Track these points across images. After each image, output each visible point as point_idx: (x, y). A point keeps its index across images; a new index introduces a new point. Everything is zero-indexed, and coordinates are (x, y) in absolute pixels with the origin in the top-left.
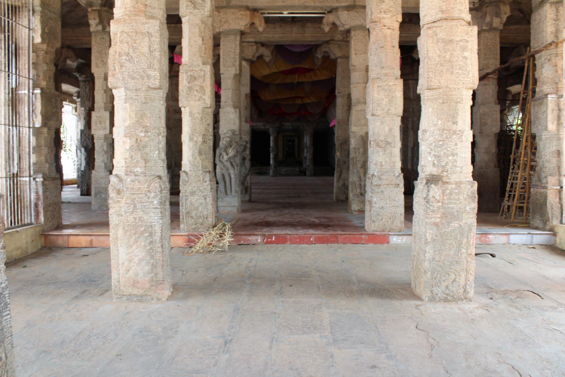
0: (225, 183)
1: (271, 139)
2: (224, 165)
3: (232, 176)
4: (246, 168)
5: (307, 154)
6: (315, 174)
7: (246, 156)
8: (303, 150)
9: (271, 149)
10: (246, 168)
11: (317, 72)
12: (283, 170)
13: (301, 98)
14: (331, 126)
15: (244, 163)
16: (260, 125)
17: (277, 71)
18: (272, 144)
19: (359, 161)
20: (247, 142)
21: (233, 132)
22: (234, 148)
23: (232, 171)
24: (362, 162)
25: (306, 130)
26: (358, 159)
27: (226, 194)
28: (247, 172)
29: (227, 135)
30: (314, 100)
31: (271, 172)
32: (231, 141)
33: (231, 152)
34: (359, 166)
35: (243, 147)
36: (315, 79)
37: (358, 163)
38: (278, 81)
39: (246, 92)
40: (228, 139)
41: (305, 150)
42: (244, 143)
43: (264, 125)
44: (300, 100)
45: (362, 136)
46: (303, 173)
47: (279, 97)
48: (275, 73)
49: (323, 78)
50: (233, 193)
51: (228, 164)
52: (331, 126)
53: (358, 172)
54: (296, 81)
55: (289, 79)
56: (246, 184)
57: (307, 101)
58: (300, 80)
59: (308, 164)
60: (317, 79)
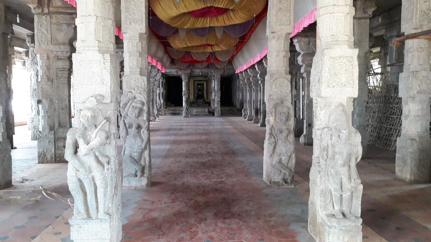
0: (85, 194)
1: (184, 84)
2: (82, 163)
3: (98, 183)
4: (143, 140)
5: (215, 97)
6: (223, 114)
7: (142, 124)
8: (212, 93)
9: (183, 93)
10: (143, 140)
11: (231, 14)
12: (194, 111)
13: (211, 46)
14: (236, 72)
15: (139, 132)
16: (173, 71)
17: (186, 11)
18: (184, 89)
19: (341, 153)
20: (143, 104)
21: (100, 99)
22: (101, 130)
23: (97, 173)
24: (345, 155)
25: (214, 76)
26: (336, 150)
27: (89, 217)
28: (143, 146)
29: (89, 105)
30: (224, 48)
31: (184, 115)
32: (94, 117)
33: (96, 138)
34: (340, 162)
35: (137, 111)
36: (228, 23)
37: (337, 156)
38: (188, 26)
39: (140, 31)
40: (89, 114)
41: (213, 94)
42: (139, 105)
43: (177, 72)
44: (210, 47)
45: (341, 105)
46: (212, 113)
47: (189, 45)
48: (184, 14)
49: (237, 22)
50: (101, 215)
51: (91, 161)
52: (236, 72)
53: (337, 173)
54: (208, 26)
55: (201, 23)
56: (142, 163)
57: (216, 49)
58: (212, 25)
59: (216, 106)
60: (231, 24)
